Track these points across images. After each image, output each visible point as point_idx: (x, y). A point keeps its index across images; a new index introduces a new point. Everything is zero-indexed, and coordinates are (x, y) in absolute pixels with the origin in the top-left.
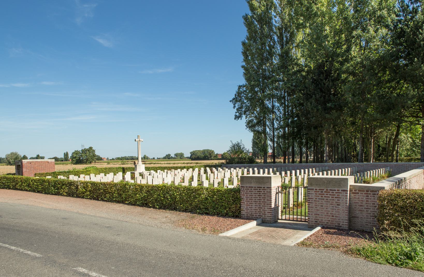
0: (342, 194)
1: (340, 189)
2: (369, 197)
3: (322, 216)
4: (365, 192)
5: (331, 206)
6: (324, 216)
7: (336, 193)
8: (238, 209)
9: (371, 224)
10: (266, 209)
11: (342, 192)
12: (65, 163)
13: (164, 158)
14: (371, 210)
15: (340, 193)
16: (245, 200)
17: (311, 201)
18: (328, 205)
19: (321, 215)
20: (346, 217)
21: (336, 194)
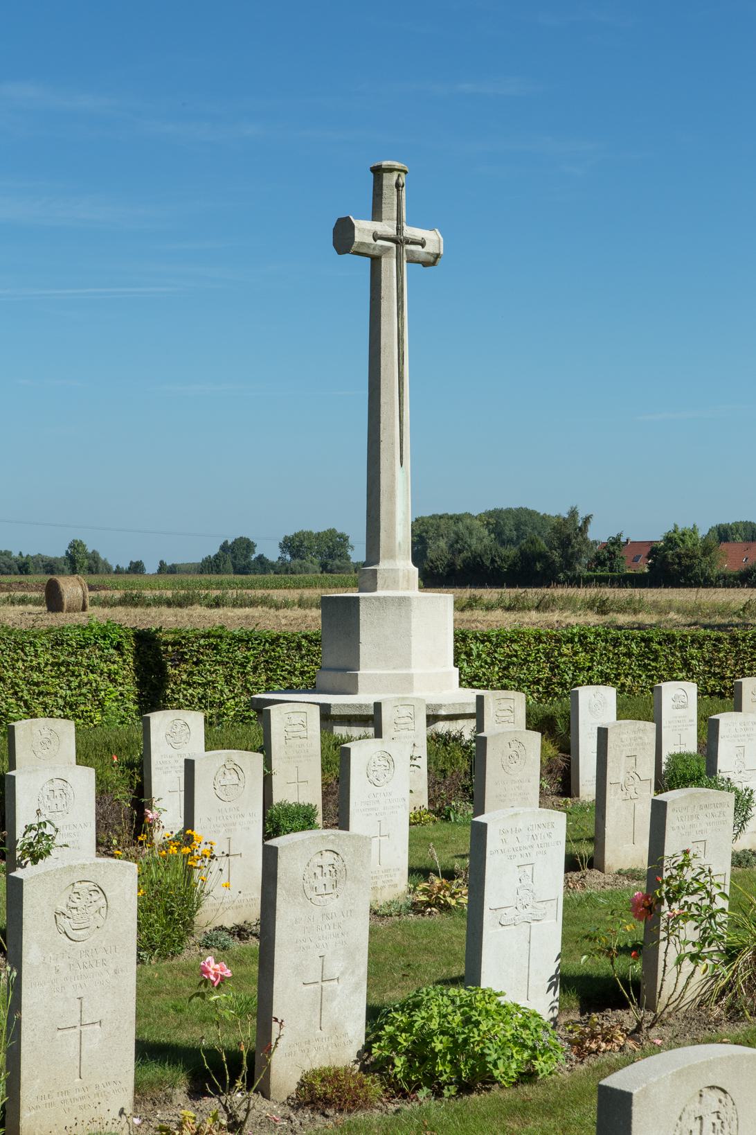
12: (721, 614)
13: (211, 566)
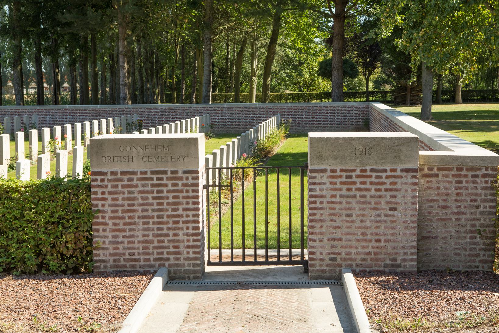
0: (404, 180)
1: (399, 167)
2: (464, 184)
3: (349, 244)
4: (455, 172)
5: (374, 213)
6: (354, 243)
7: (387, 177)
8: (85, 247)
9: (468, 252)
10: (181, 238)
11: (404, 174)
14: (468, 216)
15: (397, 177)
16: (109, 214)
17: (318, 205)
18: (366, 212)
19: (348, 240)
20: (413, 241)
21: (388, 181)
